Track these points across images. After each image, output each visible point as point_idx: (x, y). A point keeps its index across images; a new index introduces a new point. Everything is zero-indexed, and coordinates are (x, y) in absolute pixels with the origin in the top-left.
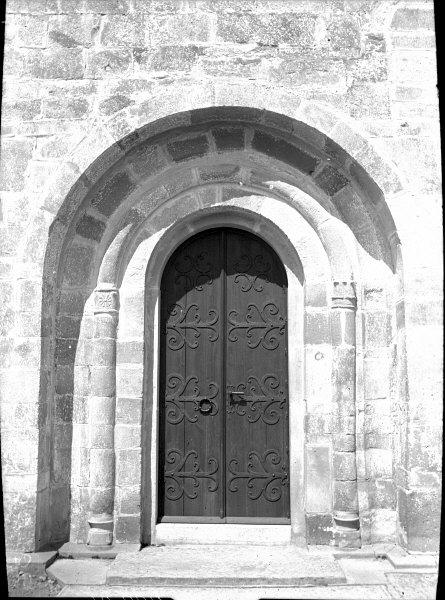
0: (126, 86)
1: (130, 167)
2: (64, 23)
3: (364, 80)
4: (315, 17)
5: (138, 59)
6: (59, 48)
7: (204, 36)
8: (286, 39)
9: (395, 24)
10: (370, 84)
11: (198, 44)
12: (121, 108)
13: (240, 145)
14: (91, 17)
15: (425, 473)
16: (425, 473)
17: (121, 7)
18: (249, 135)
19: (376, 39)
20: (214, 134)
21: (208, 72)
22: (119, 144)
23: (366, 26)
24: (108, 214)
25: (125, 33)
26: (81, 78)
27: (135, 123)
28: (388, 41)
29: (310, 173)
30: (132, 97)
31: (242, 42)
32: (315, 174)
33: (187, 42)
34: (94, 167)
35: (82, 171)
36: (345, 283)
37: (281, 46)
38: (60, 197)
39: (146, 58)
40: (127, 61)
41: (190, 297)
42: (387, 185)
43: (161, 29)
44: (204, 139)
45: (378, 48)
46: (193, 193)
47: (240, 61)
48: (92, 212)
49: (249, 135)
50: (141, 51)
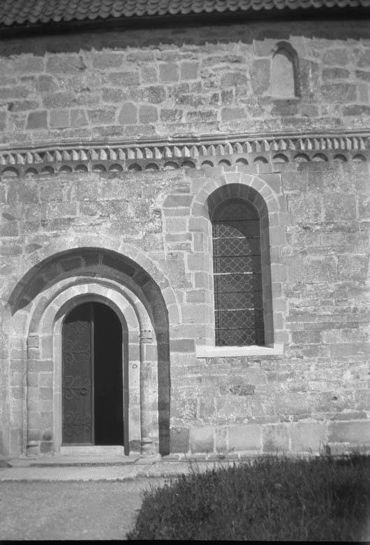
0: (37, 238)
1: (43, 275)
2: (9, 209)
3: (151, 232)
4: (128, 202)
5: (43, 225)
6: (7, 222)
7: (74, 213)
8: (114, 213)
9: (165, 204)
10: (153, 234)
11: (72, 217)
12: (35, 249)
13: (97, 262)
14: (21, 205)
15: (178, 419)
16: (178, 419)
17: (35, 200)
18: (101, 257)
19: (157, 212)
20: (83, 257)
21: (77, 231)
22: (36, 266)
23: (152, 206)
24: (214, 276)
25: (37, 214)
26: (17, 236)
27: (42, 256)
28: (163, 212)
29: (132, 275)
30: (40, 244)
31: (92, 215)
32: (134, 276)
33: (66, 216)
34: (25, 278)
35: (18, 281)
36: (150, 331)
37: (111, 216)
38: (8, 293)
39: (47, 224)
40: (38, 226)
41: (18, 312)
42: (161, 284)
43: (54, 210)
44: (79, 260)
45: (157, 216)
46: (75, 289)
47: (91, 224)
48: (25, 297)
49: (101, 257)
50: (44, 221)
